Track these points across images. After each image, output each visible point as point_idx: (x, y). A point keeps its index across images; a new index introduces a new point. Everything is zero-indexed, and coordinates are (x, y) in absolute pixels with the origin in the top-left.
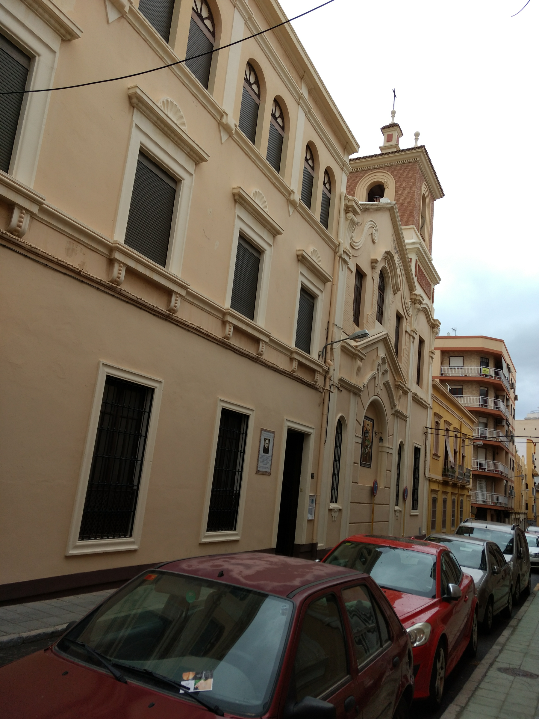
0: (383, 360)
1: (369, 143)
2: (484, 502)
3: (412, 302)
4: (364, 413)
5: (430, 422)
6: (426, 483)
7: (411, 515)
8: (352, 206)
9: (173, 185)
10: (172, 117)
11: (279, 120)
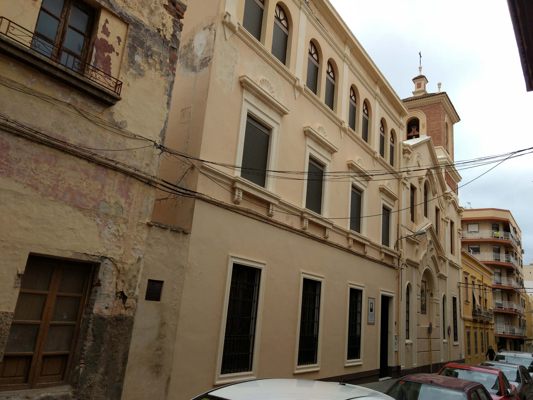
0: (430, 242)
1: (404, 90)
2: (504, 332)
3: (444, 198)
4: (421, 278)
5: (461, 279)
6: (462, 322)
7: (454, 345)
8: (407, 150)
9: (266, 131)
10: (265, 89)
11: (315, 56)
